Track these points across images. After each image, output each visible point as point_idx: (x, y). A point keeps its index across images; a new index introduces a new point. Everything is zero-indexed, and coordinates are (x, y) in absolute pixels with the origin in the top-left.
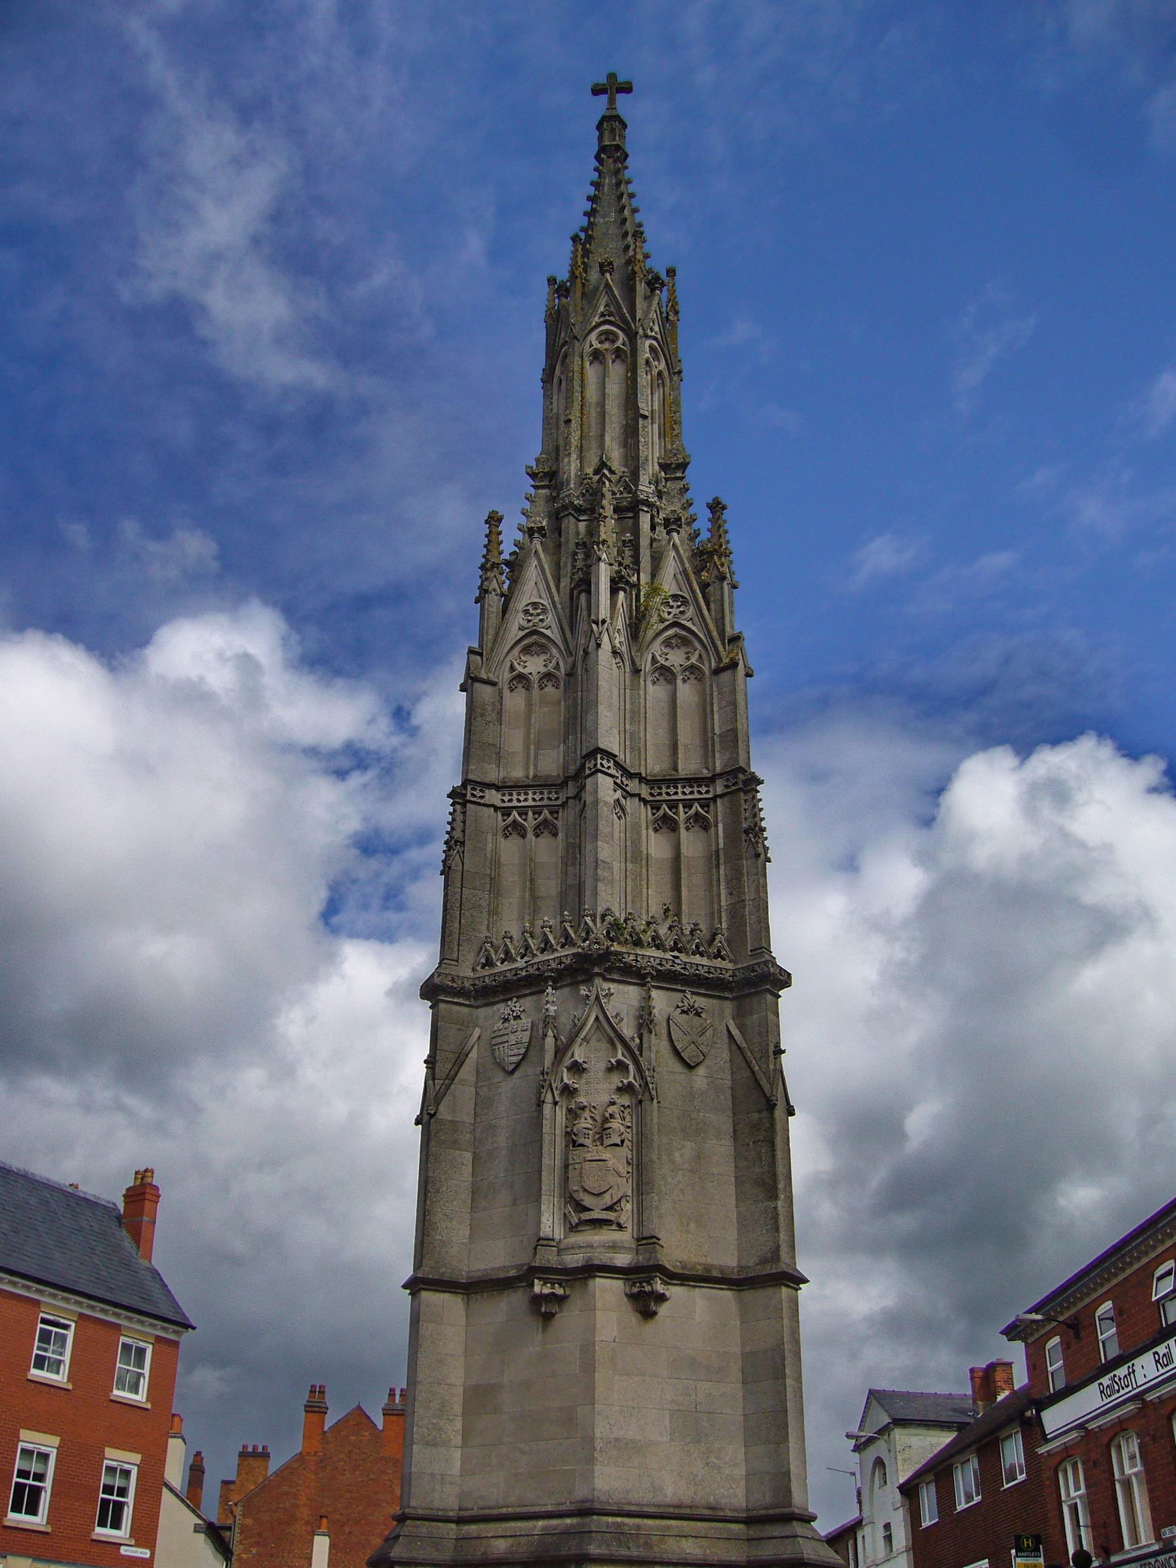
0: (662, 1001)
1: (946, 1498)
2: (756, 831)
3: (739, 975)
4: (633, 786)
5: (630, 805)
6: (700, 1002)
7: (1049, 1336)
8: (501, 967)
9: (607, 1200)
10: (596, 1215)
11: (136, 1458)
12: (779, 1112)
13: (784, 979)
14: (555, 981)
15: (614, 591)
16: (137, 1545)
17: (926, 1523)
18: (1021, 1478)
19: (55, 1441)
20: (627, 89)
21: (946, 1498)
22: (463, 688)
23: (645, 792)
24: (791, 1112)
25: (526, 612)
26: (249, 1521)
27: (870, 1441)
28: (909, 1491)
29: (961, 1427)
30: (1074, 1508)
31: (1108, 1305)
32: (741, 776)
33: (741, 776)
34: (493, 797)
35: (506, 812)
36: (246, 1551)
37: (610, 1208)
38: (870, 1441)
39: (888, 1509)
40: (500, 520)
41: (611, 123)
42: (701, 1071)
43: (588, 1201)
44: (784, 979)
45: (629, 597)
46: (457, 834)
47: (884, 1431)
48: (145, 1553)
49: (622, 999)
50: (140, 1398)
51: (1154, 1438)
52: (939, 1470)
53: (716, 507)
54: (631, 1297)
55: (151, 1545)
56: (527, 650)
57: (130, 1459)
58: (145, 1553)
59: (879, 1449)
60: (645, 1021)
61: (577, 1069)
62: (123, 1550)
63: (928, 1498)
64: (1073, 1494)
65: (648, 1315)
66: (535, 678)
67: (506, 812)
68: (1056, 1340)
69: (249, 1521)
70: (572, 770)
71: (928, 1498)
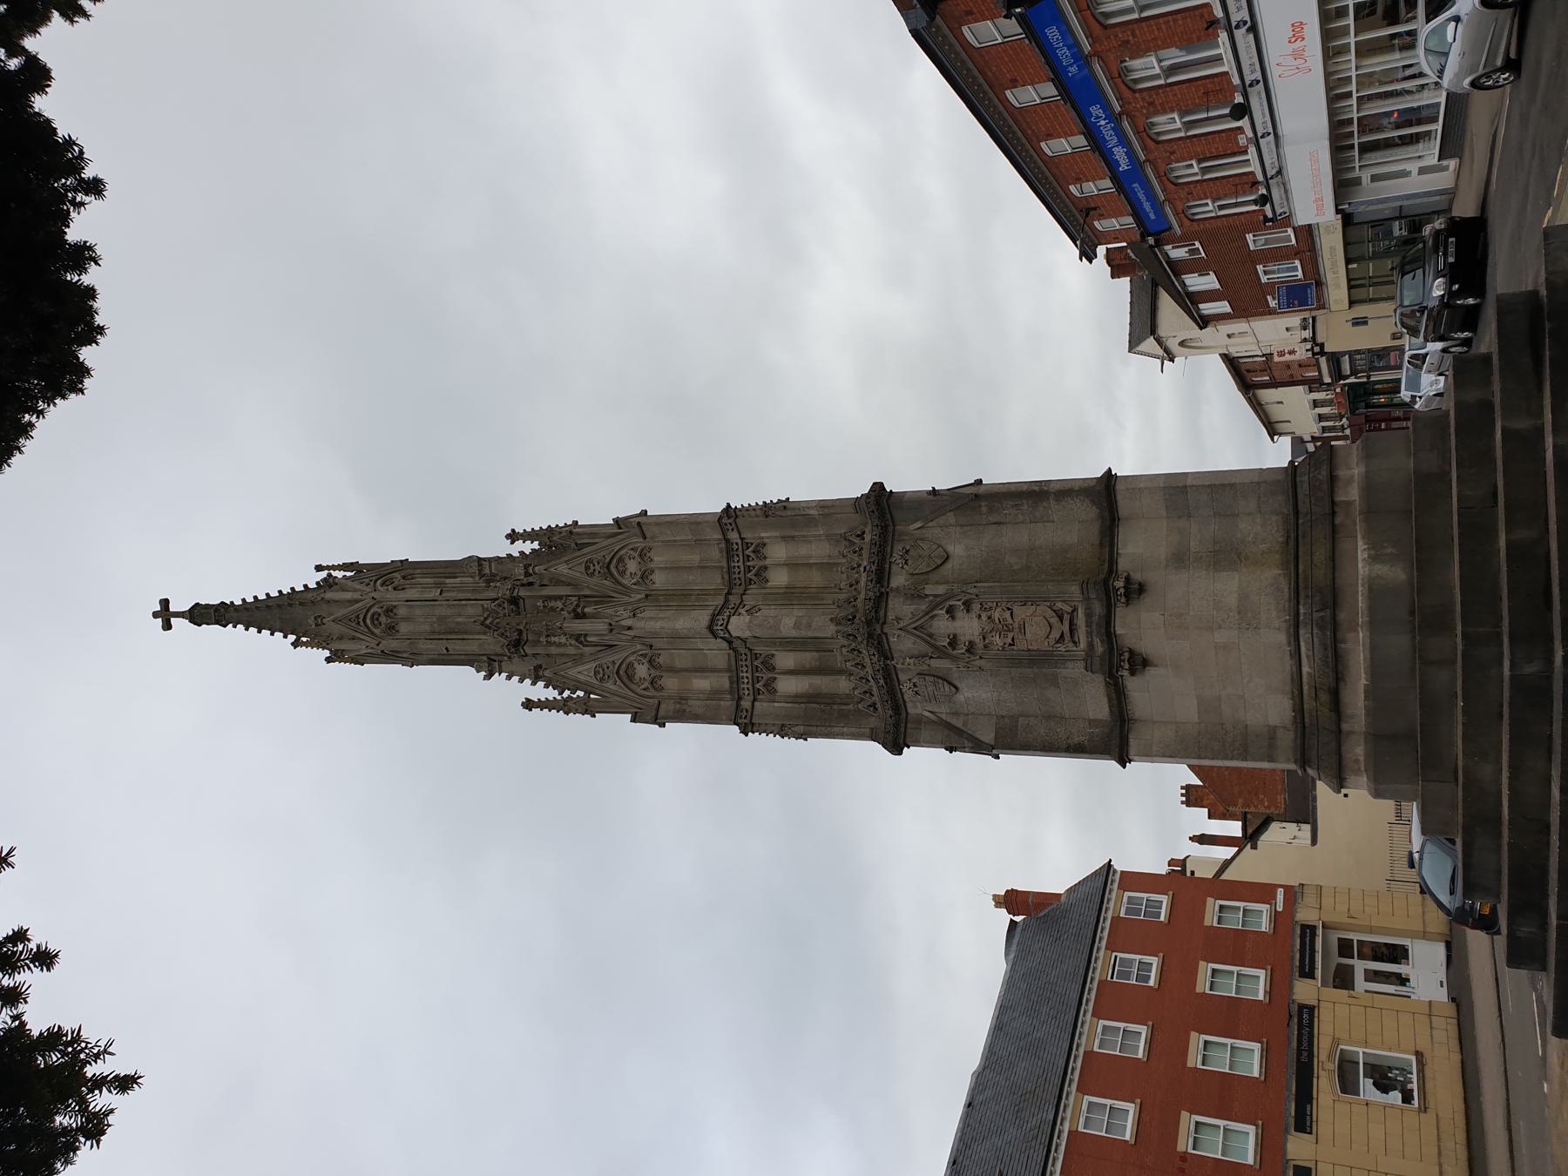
0: (898, 580)
1: (1210, 296)
2: (767, 509)
3: (876, 522)
4: (734, 600)
5: (749, 601)
6: (898, 548)
7: (1094, 229)
8: (876, 698)
9: (1054, 620)
10: (1066, 628)
11: (1210, 900)
12: (981, 490)
13: (878, 488)
14: (886, 658)
15: (583, 616)
16: (1275, 898)
17: (1228, 309)
18: (1197, 245)
19: (1202, 964)
20: (165, 603)
21: (1210, 296)
22: (663, 725)
23: (737, 590)
24: (979, 482)
25: (602, 680)
26: (1240, 801)
27: (1167, 351)
28: (1204, 322)
29: (1155, 285)
30: (1221, 207)
31: (1072, 188)
32: (724, 521)
33: (724, 521)
34: (746, 704)
35: (757, 692)
36: (1262, 802)
37: (1061, 618)
38: (1167, 351)
39: (1215, 335)
40: (528, 700)
41: (200, 615)
42: (950, 548)
43: (1056, 635)
44: (878, 488)
45: (588, 604)
46: (776, 729)
47: (1159, 341)
48: (1280, 893)
49: (900, 609)
50: (1165, 900)
51: (1172, 153)
52: (1189, 302)
53: (513, 537)
54: (1127, 604)
55: (1274, 887)
56: (631, 678)
57: (1212, 905)
58: (1280, 893)
59: (1173, 344)
60: (915, 595)
61: (953, 642)
62: (1280, 909)
63: (1208, 308)
64: (1210, 207)
65: (1142, 589)
66: (653, 672)
67: (757, 692)
68: (1096, 224)
69: (1240, 801)
70: (725, 645)
71: (1208, 308)
